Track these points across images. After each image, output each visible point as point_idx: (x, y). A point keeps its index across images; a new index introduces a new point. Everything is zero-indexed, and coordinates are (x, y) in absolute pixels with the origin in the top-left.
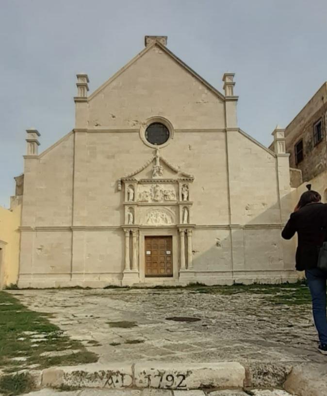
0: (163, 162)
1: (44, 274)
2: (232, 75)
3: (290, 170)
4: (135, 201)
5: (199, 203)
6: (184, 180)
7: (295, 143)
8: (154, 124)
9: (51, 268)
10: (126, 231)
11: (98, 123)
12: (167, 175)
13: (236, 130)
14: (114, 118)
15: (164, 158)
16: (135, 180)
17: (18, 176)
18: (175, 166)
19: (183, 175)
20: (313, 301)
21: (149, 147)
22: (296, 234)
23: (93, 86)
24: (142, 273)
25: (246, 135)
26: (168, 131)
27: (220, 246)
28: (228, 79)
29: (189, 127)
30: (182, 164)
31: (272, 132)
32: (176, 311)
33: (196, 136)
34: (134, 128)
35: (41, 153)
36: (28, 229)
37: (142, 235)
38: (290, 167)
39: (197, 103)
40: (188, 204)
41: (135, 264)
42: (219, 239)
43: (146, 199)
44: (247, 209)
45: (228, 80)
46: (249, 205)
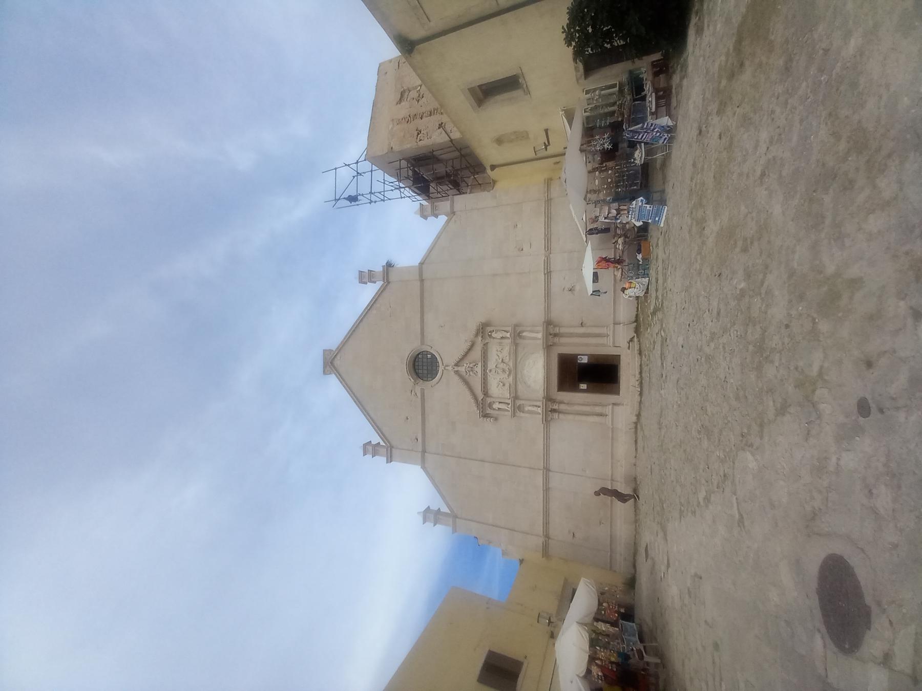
1: (426, 14)
2: (360, 272)
3: (469, 193)
4: (509, 401)
6: (482, 337)
8: (417, 374)
9: (602, 525)
10: (551, 409)
12: (477, 353)
16: (482, 400)
17: (366, 146)
18: (464, 347)
19: (477, 335)
20: (633, 59)
23: (376, 439)
26: (423, 352)
28: (366, 277)
29: (418, 327)
31: (424, 220)
32: (721, 431)
33: (429, 317)
34: (419, 394)
35: (447, 509)
39: (390, 316)
40: (514, 332)
41: (598, 409)
44: (522, 250)
45: (366, 280)
46: (516, 247)
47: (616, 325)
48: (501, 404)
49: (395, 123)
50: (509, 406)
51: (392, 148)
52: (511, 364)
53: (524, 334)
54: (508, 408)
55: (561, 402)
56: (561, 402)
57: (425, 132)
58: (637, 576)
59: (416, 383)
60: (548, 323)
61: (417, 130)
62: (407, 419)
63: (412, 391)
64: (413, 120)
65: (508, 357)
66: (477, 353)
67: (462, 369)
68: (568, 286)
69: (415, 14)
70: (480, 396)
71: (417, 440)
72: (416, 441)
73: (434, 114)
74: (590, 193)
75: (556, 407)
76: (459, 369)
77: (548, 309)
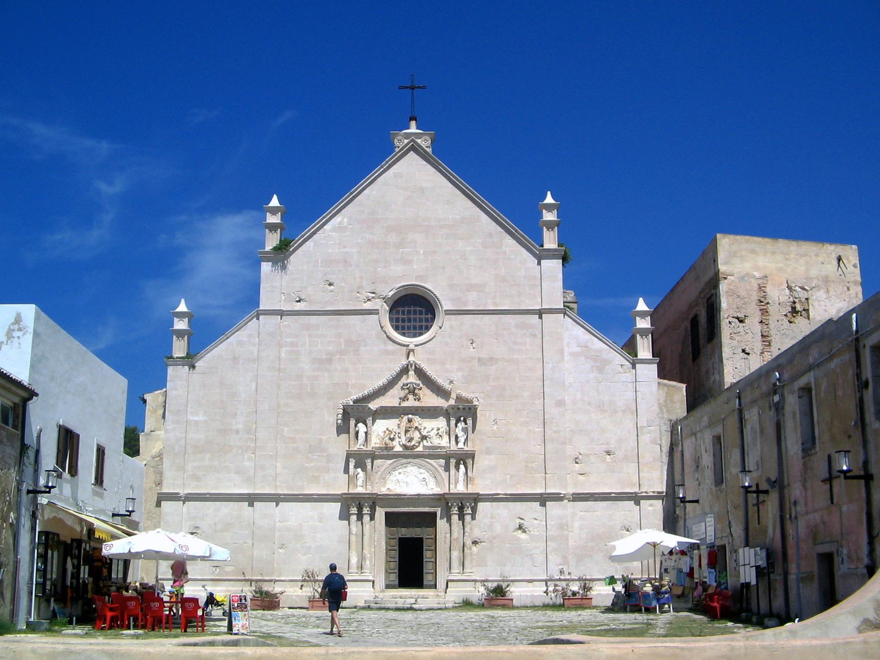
0: (420, 373)
5: (488, 452)
7: (856, 391)
11: (303, 297)
12: (429, 399)
13: (535, 314)
14: (332, 287)
15: (425, 366)
21: (394, 342)
22: (549, 193)
24: (381, 582)
25: (16, 537)
27: (524, 532)
30: (457, 376)
34: (368, 306)
36: (173, 497)
37: (380, 513)
38: (563, 289)
42: (522, 519)
43: (391, 444)
44: (577, 463)
47: (372, 583)
48: (364, 435)
49: (760, 282)
50: (362, 447)
51: (725, 278)
52: (420, 449)
53: (462, 467)
54: (360, 446)
55: (372, 518)
56: (372, 518)
57: (741, 329)
58: (54, 634)
59: (386, 300)
60: (477, 499)
61: (745, 316)
62: (330, 284)
63: (374, 293)
64: (761, 310)
65: (430, 445)
66: (429, 399)
67: (412, 378)
68: (526, 524)
69: (661, 466)
70: (373, 405)
71: (298, 301)
72: (298, 299)
73: (764, 341)
74: (232, 630)
75: (366, 510)
76: (412, 373)
77: (494, 498)
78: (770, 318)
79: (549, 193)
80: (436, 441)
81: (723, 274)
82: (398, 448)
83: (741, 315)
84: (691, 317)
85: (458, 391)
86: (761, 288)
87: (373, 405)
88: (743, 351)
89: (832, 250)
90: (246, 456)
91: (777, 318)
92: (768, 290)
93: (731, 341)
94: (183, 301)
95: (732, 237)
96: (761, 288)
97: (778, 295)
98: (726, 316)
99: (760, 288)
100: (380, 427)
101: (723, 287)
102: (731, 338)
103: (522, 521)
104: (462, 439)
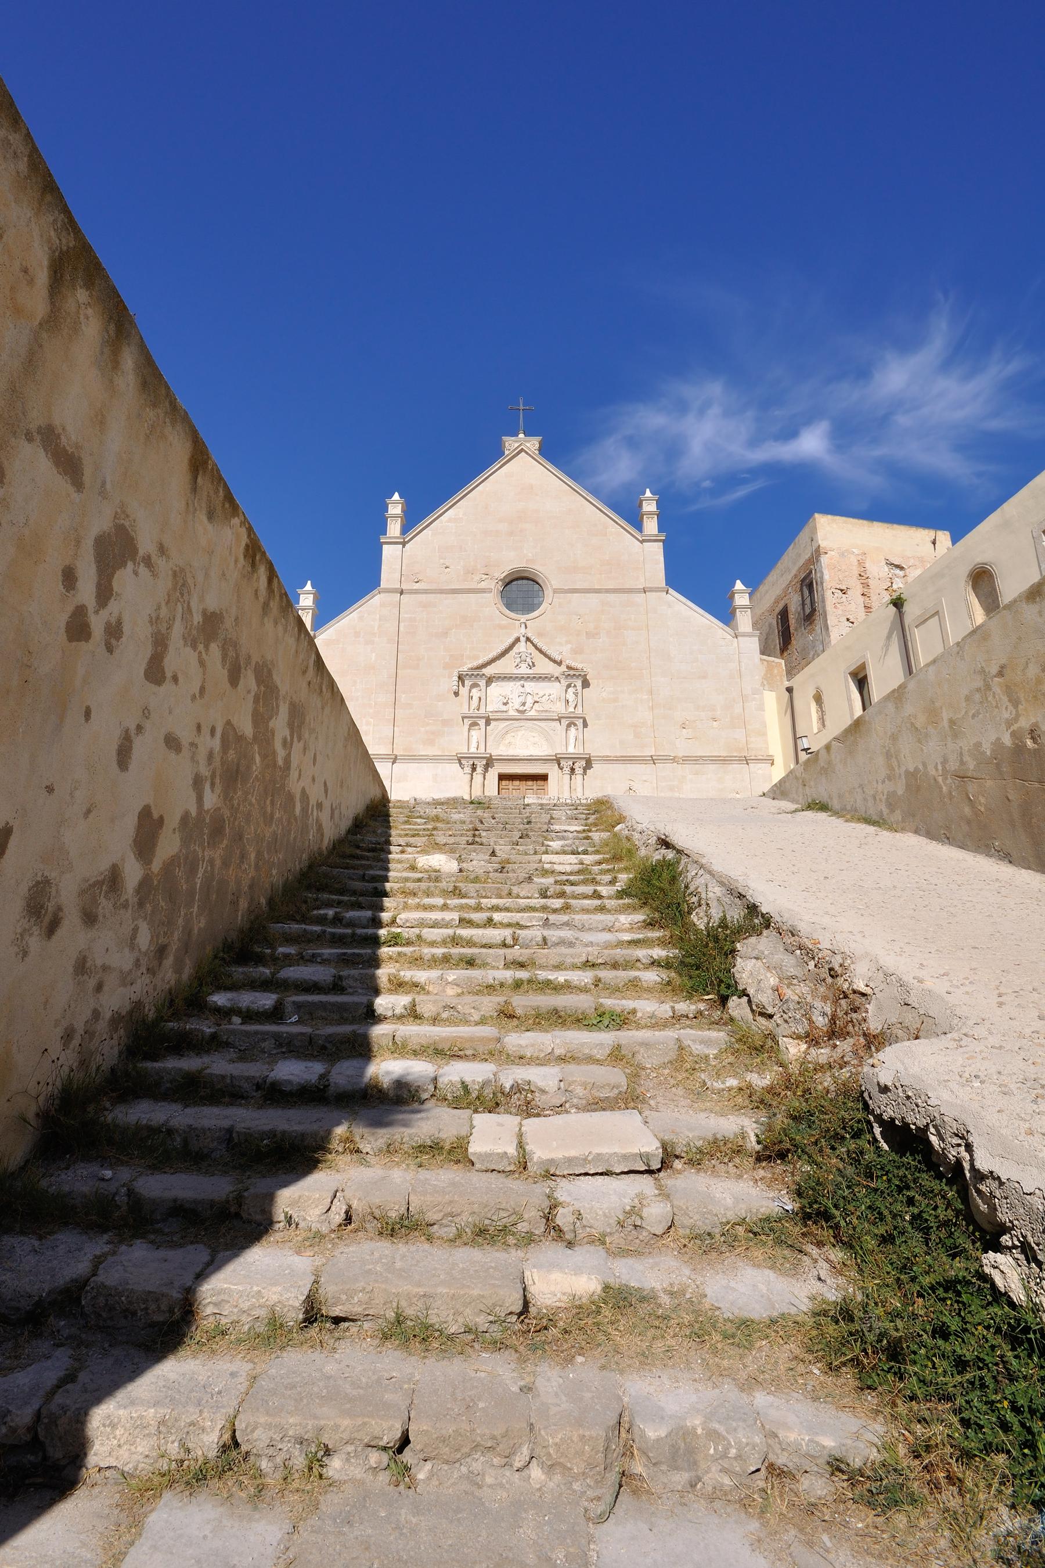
22: (309, 582)
49: (860, 558)
66: (544, 667)
70: (488, 671)
75: (479, 770)
78: (871, 591)
79: (309, 582)
80: (547, 706)
81: (823, 548)
82: (512, 713)
83: (844, 587)
84: (778, 610)
85: (567, 662)
86: (861, 563)
87: (488, 671)
88: (848, 620)
89: (926, 535)
90: (364, 721)
91: (878, 591)
92: (867, 565)
93: (835, 610)
94: (309, 582)
95: (829, 517)
96: (861, 563)
97: (878, 571)
98: (829, 587)
99: (860, 564)
100: (496, 690)
101: (824, 560)
102: (835, 607)
103: (632, 783)
104: (572, 704)
